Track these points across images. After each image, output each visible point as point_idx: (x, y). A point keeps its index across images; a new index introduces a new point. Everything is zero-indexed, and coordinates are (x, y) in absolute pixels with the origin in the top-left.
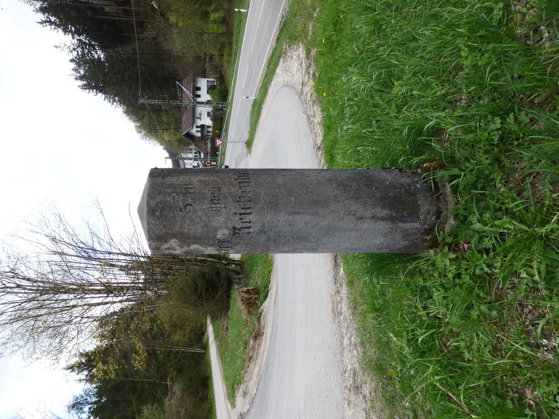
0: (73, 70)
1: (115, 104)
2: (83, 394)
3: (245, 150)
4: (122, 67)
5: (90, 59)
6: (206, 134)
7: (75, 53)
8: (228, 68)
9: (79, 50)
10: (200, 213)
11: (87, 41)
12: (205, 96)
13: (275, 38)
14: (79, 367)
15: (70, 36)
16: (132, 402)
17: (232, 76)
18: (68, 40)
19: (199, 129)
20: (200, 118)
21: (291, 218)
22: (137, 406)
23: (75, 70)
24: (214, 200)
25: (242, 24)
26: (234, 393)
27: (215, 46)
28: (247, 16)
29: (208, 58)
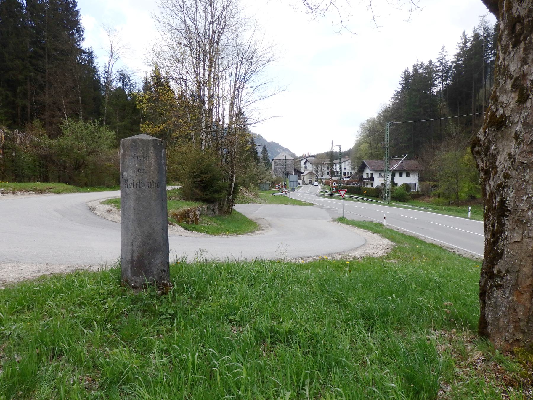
0: (422, 63)
1: (393, 100)
2: (132, 82)
3: (337, 217)
4: (426, 105)
5: (432, 78)
6: (366, 182)
7: (438, 64)
8: (427, 202)
9: (442, 68)
10: (133, 163)
11: (449, 75)
12: (400, 181)
13: (434, 243)
14: (157, 76)
15: (454, 60)
16: (123, 122)
17: (416, 206)
18: (451, 58)
19: (370, 176)
20: (380, 176)
21: (132, 208)
22: (119, 126)
23: (422, 65)
24: (140, 170)
25: (456, 213)
26: (112, 203)
27: (446, 190)
28: (465, 218)
29: (435, 183)
